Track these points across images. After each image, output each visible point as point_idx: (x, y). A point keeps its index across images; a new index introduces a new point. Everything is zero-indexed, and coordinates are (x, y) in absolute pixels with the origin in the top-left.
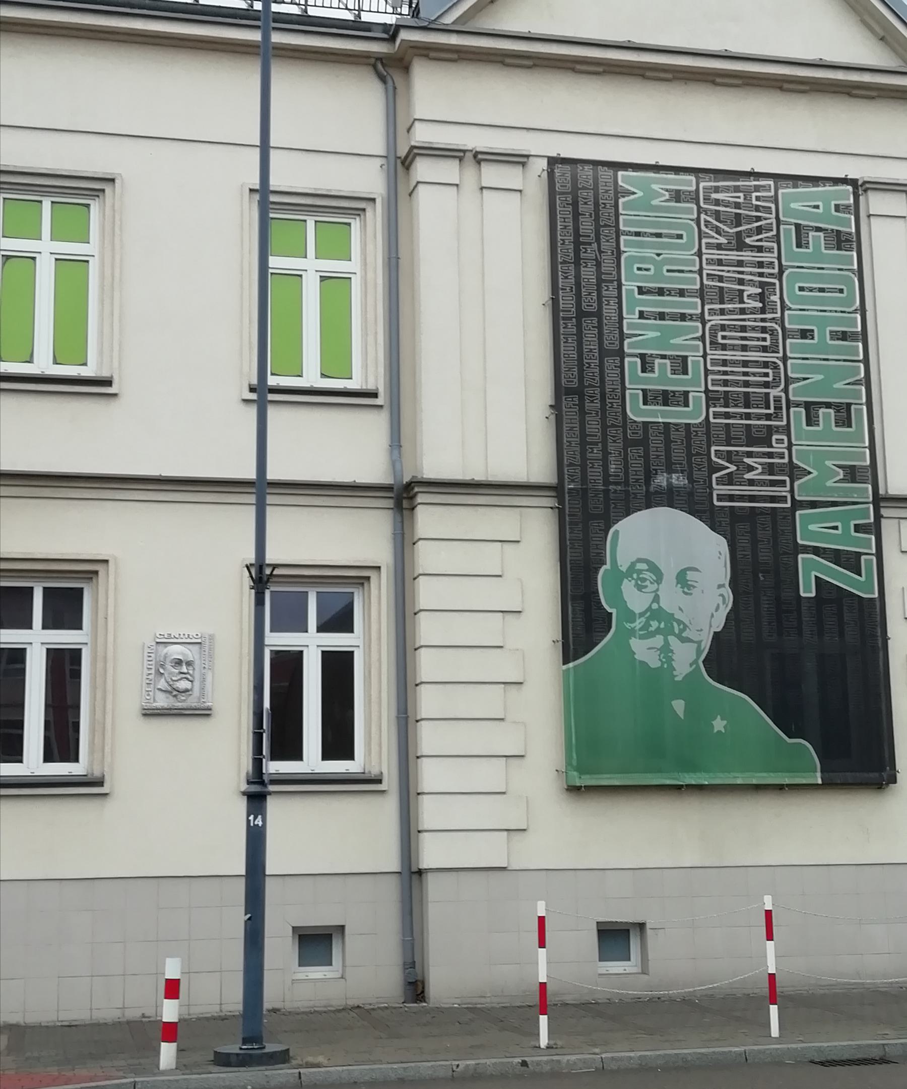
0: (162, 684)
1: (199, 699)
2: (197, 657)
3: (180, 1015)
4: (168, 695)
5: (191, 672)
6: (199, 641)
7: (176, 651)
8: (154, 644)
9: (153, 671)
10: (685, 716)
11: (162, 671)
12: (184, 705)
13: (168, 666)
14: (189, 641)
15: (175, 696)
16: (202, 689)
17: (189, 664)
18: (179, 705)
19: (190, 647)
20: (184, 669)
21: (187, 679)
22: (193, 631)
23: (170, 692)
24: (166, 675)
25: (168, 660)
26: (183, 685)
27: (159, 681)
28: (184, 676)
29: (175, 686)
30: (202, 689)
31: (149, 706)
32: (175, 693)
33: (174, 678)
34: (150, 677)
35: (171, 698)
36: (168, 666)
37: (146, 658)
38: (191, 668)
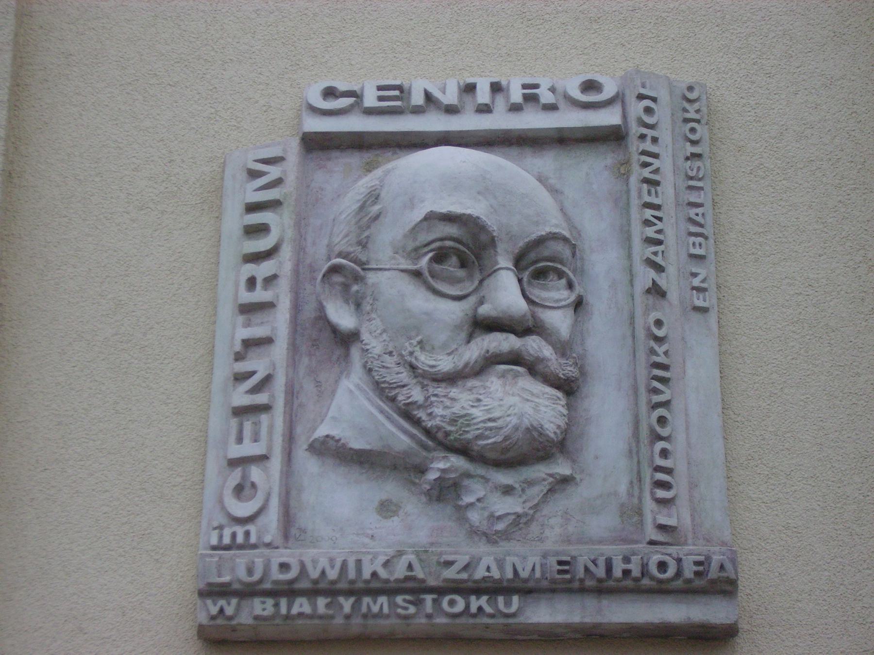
0: (349, 410)
1: (632, 512)
2: (595, 226)
3: (626, 146)
4: (390, 488)
5: (559, 321)
6: (610, 118)
7: (439, 180)
8: (294, 147)
9: (279, 323)
10: (327, 597)
11: (343, 317)
12: (525, 558)
13: (395, 290)
14: (533, 120)
15: (445, 492)
16: (653, 428)
17: (539, 262)
18: (488, 562)
19: (547, 162)
20: (506, 294)
21: (533, 368)
22: (558, 65)
23: (407, 468)
24: (374, 342)
25: (388, 237)
26: (511, 403)
27: (325, 393)
28: (504, 342)
29: (438, 414)
30: (653, 428)
31: (238, 568)
32: (444, 464)
33: (424, 360)
34: (258, 364)
35: (413, 506)
36: (395, 290)
37: (234, 245)
38: (555, 293)
